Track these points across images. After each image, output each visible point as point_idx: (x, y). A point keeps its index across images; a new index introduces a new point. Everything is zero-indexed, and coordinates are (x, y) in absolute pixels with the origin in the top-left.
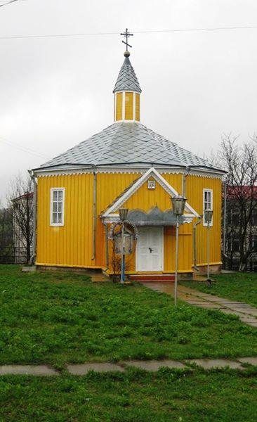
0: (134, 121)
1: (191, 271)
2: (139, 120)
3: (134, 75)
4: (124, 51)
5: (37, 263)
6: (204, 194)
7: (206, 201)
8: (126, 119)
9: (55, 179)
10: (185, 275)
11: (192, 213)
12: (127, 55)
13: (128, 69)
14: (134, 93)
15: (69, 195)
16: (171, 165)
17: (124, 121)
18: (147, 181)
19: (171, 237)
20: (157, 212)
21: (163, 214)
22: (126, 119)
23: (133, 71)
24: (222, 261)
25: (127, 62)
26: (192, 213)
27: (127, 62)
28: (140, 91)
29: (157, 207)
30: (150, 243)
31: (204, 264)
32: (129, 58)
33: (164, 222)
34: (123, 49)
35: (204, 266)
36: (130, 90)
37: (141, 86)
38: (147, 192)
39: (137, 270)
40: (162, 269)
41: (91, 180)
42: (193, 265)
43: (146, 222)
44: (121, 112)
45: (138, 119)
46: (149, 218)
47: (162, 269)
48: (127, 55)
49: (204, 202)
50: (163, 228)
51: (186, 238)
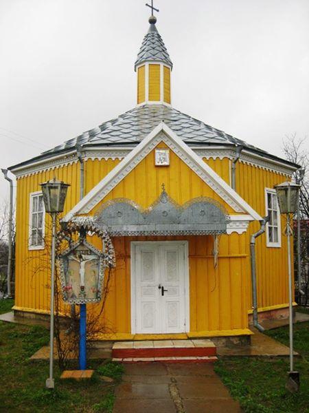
0: (161, 102)
1: (247, 332)
2: (169, 102)
3: (162, 45)
4: (149, 16)
5: (15, 308)
6: (266, 195)
7: (269, 207)
8: (149, 100)
9: (36, 176)
10: (236, 342)
11: (247, 213)
12: (153, 21)
13: (154, 43)
14: (162, 65)
15: (21, 193)
16: (210, 144)
17: (147, 102)
18: (153, 151)
19: (205, 261)
20: (164, 206)
21: (181, 210)
22: (149, 100)
23: (160, 40)
24: (296, 301)
25: (153, 29)
26: (247, 213)
27: (153, 29)
28: (171, 65)
29: (164, 193)
30: (159, 274)
31: (269, 308)
32: (156, 24)
33: (181, 227)
34: (148, 14)
35: (269, 311)
36: (154, 60)
37: (172, 58)
38: (153, 172)
39: (133, 333)
40: (188, 331)
41: (79, 172)
42: (251, 311)
43: (141, 228)
44: (144, 91)
45: (168, 100)
46: (147, 217)
47: (188, 331)
48: (153, 21)
49: (267, 209)
50: (184, 248)
51: (236, 263)
